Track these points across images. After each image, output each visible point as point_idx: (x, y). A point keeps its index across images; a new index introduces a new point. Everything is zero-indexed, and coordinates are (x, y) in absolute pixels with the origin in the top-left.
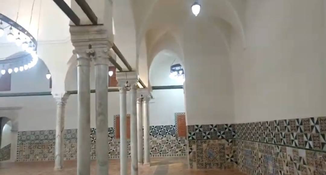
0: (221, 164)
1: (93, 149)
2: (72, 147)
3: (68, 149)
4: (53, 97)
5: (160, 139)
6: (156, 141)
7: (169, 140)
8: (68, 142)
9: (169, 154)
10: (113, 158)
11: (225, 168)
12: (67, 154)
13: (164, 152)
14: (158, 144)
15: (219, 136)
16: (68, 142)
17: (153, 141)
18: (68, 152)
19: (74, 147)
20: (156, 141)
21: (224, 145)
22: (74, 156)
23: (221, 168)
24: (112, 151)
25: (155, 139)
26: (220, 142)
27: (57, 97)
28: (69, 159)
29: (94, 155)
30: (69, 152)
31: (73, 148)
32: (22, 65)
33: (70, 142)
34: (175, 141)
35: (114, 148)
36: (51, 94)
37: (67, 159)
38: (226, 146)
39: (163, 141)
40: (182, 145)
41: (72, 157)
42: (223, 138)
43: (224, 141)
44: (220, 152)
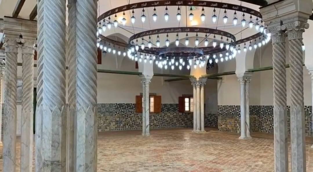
0: (254, 129)
1: (124, 121)
2: (106, 120)
3: (103, 122)
4: (236, 75)
5: (172, 114)
6: (169, 116)
7: (178, 115)
8: (102, 115)
9: (177, 125)
10: (124, 130)
11: (256, 131)
12: (102, 126)
13: (175, 124)
14: (171, 118)
15: (267, 113)
16: (102, 115)
17: (168, 116)
18: (102, 124)
19: (108, 120)
20: (169, 116)
21: (255, 118)
22: (108, 127)
23: (254, 131)
24: (138, 123)
25: (169, 114)
26: (254, 116)
27: (148, 77)
28: (104, 130)
29: (124, 127)
30: (104, 124)
31: (108, 121)
32: (261, 42)
33: (104, 116)
34: (181, 116)
35: (140, 121)
36: (235, 74)
37: (102, 130)
38: (257, 119)
39: (174, 116)
40: (186, 119)
41: (106, 128)
42: (255, 114)
43: (256, 116)
44: (254, 122)
